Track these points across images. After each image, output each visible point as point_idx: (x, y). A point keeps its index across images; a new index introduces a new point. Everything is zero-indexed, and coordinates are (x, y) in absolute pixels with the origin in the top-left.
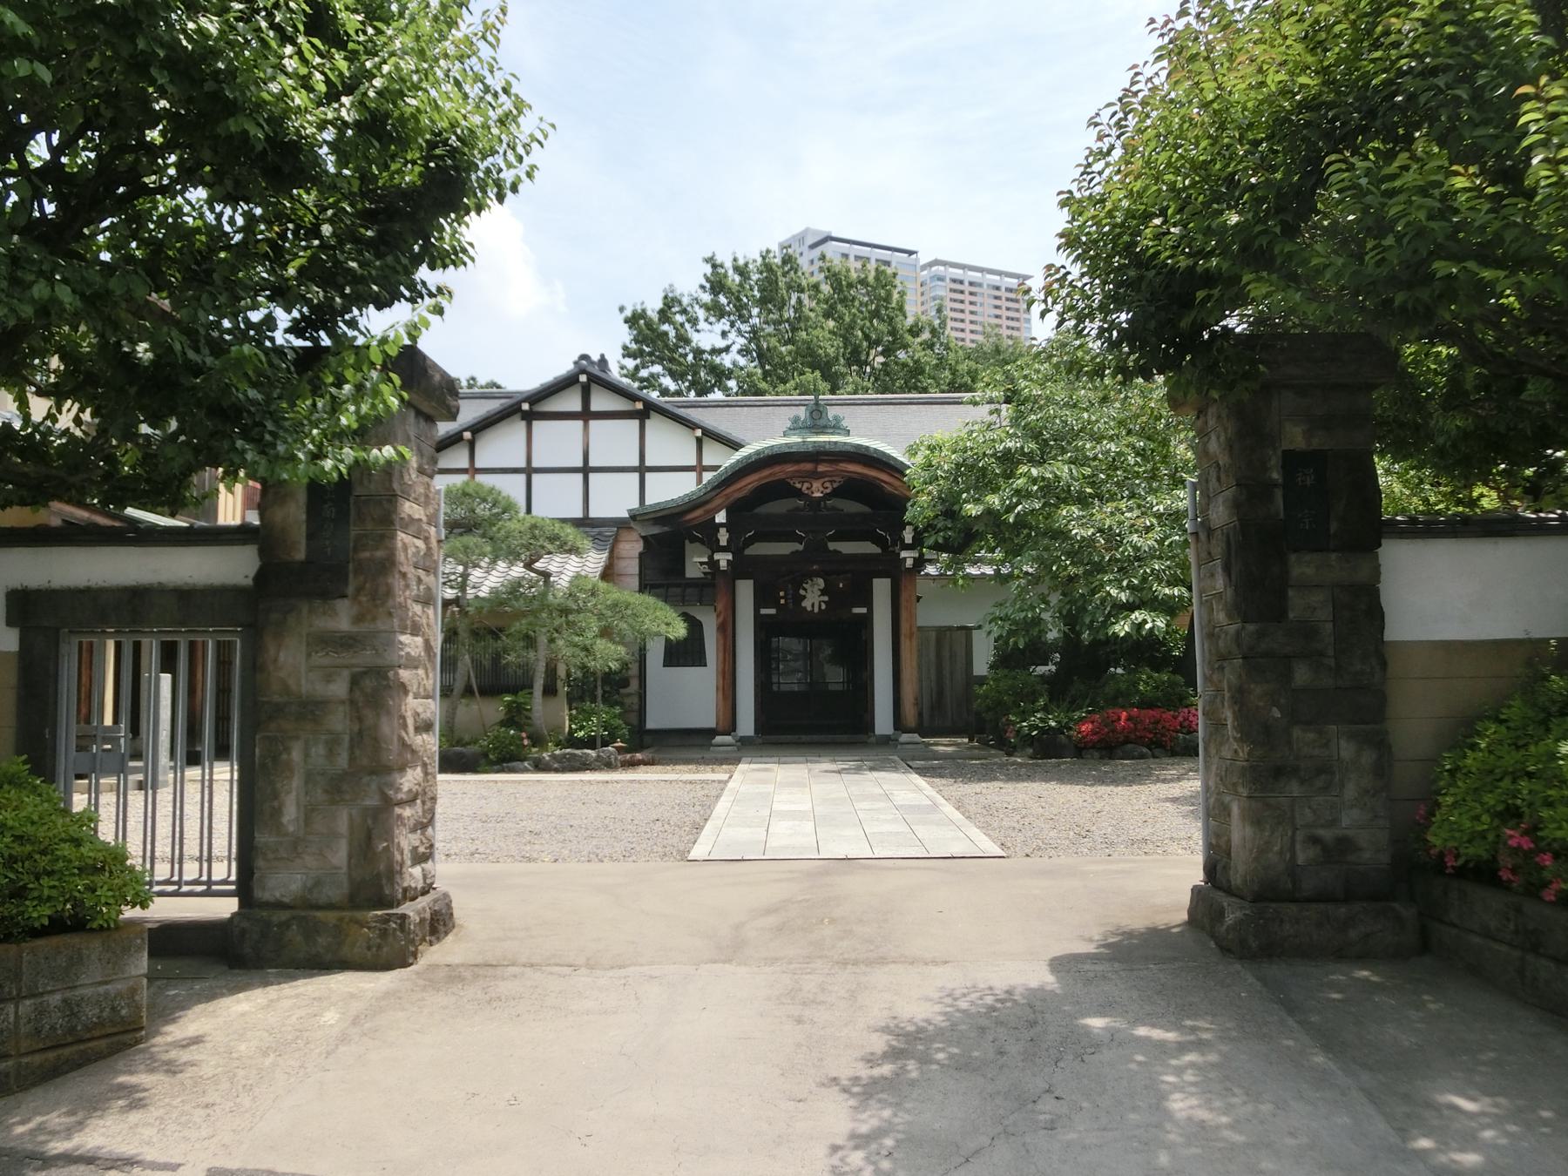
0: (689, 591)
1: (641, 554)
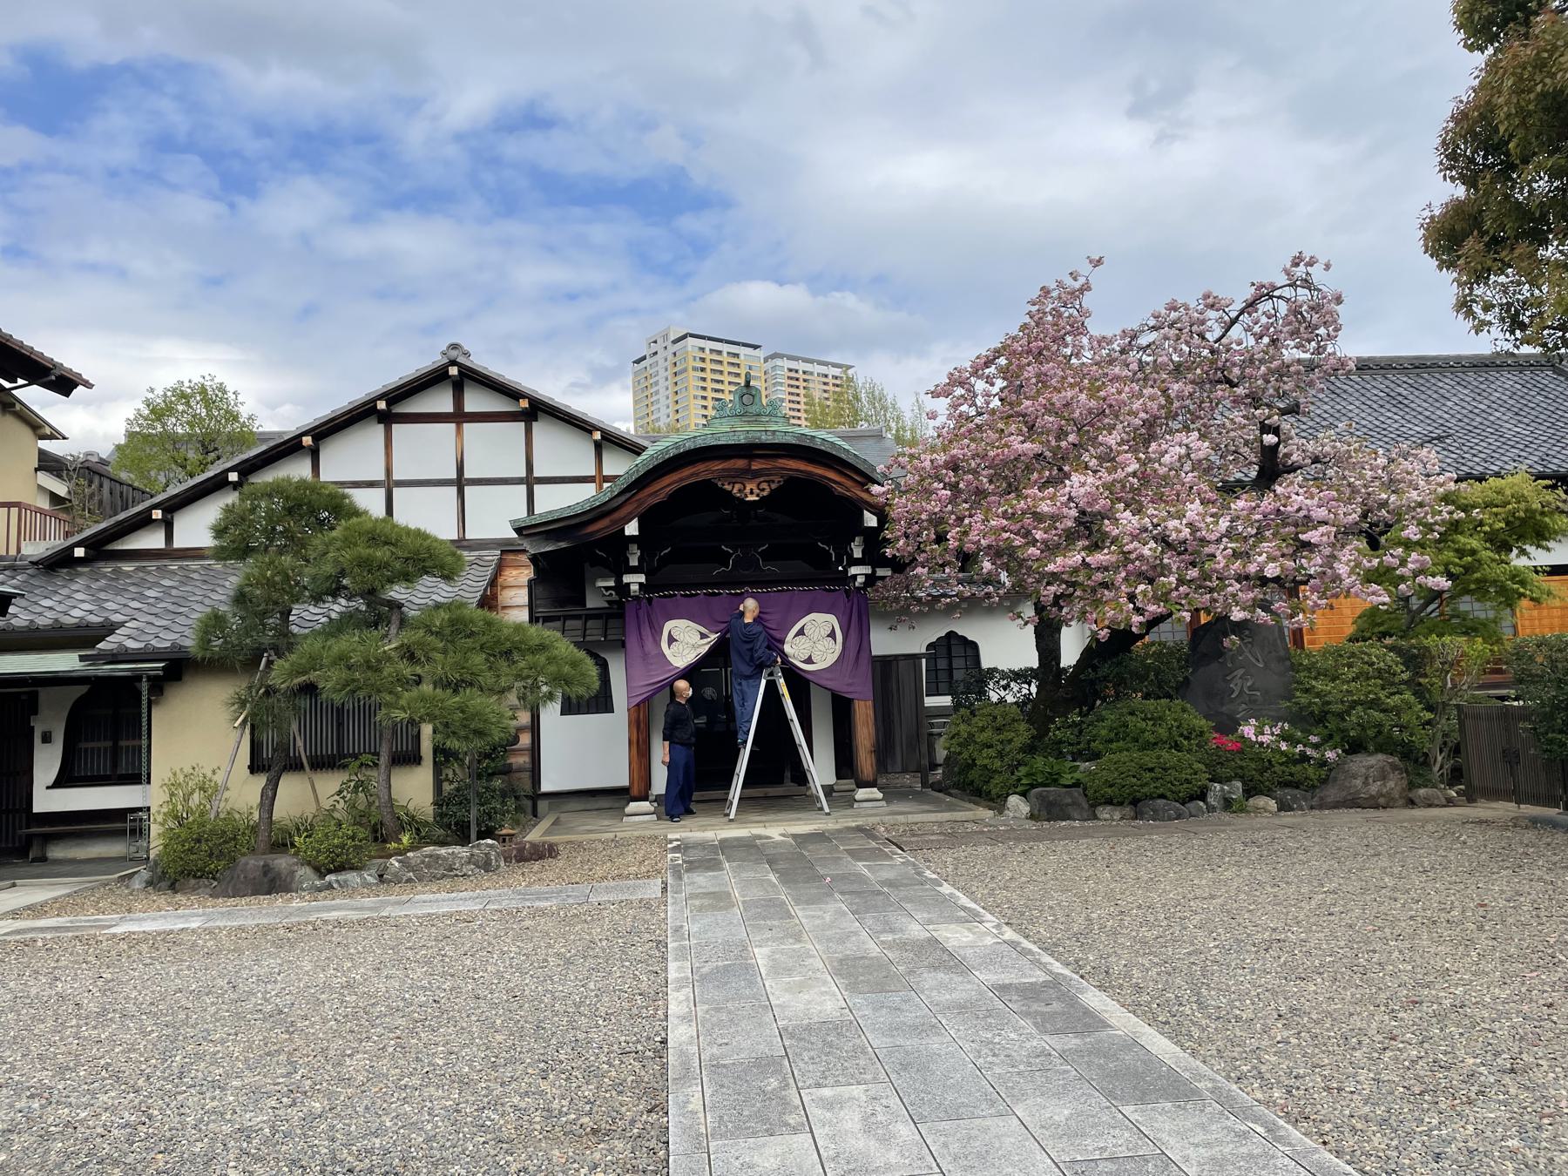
0: (590, 623)
1: (530, 581)
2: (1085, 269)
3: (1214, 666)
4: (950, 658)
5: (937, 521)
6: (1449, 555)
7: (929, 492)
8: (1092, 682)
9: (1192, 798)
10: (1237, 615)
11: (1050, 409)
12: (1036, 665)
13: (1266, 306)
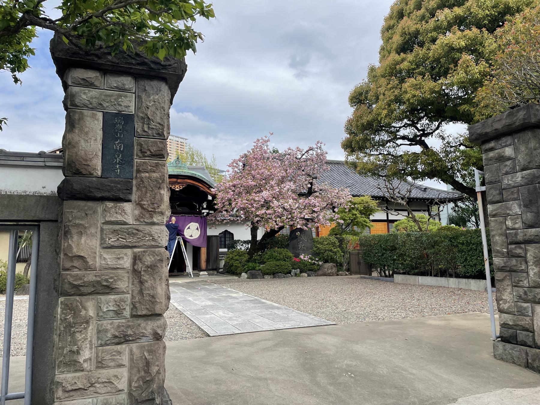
2: (269, 135)
3: (295, 241)
4: (225, 238)
5: (230, 200)
6: (350, 215)
7: (228, 192)
8: (265, 244)
9: (288, 273)
10: (299, 227)
11: (258, 174)
12: (250, 239)
13: (311, 152)
